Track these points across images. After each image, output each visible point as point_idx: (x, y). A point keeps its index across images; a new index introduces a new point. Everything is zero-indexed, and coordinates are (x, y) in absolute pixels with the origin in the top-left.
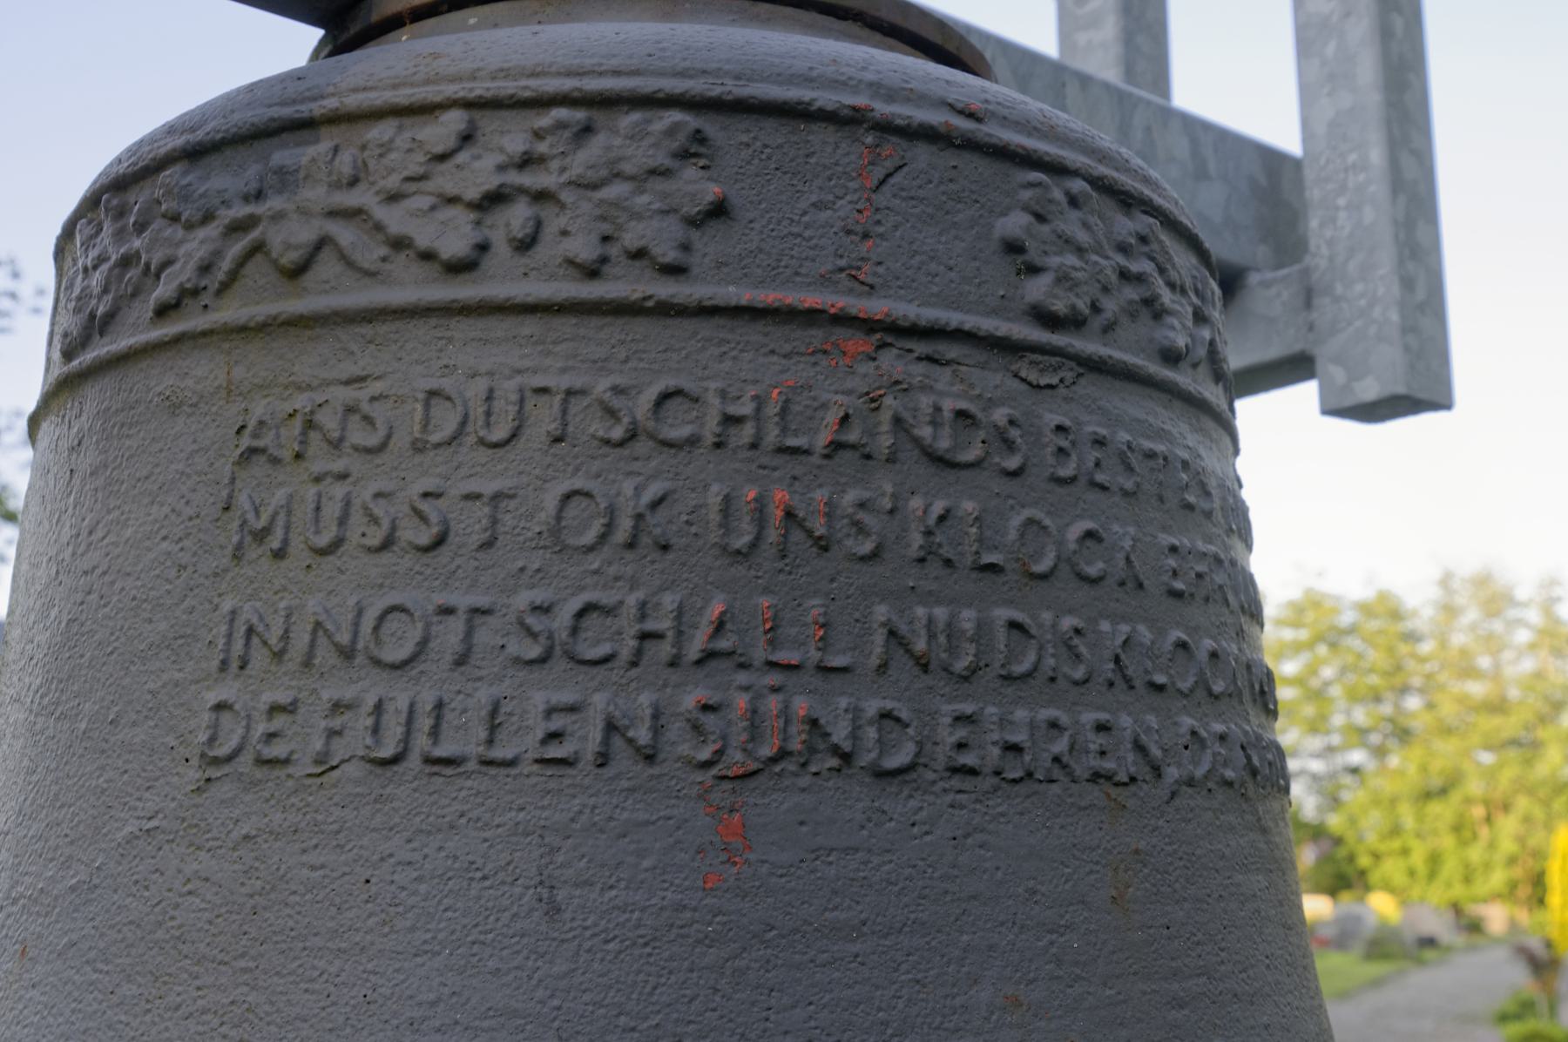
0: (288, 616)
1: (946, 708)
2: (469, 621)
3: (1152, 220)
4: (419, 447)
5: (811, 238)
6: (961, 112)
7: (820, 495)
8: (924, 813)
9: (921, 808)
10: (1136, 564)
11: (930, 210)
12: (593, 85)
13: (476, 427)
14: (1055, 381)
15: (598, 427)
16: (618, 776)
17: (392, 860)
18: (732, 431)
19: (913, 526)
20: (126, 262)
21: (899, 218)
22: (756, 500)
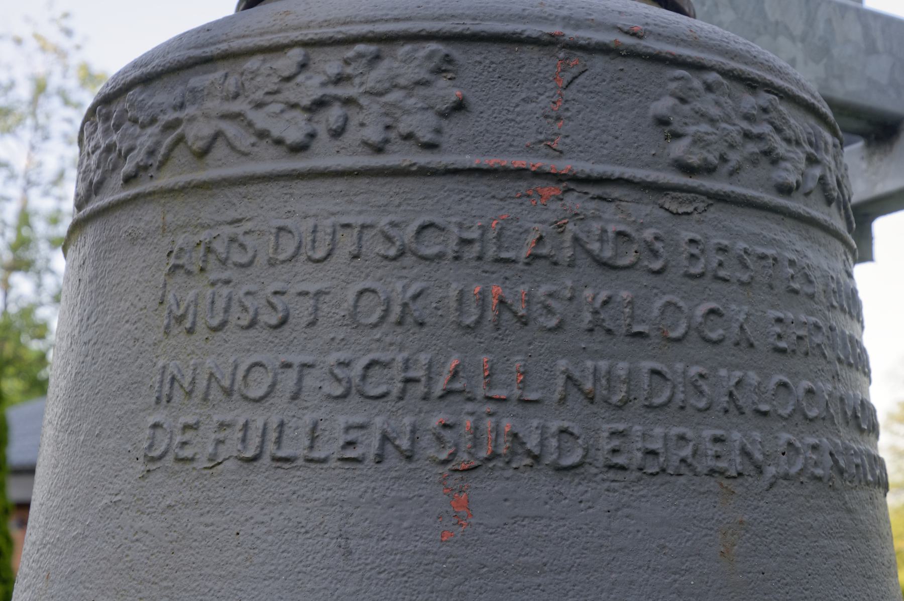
0: (195, 370)
1: (606, 426)
2: (300, 372)
3: (772, 96)
4: (272, 263)
5: (521, 122)
6: (627, 33)
7: (523, 289)
8: (589, 495)
9: (586, 491)
10: (748, 331)
11: (603, 100)
12: (381, 28)
13: (307, 251)
14: (690, 209)
15: (381, 248)
16: (389, 469)
17: (252, 521)
18: (466, 248)
19: (585, 308)
20: (109, 149)
21: (582, 106)
22: (480, 293)
